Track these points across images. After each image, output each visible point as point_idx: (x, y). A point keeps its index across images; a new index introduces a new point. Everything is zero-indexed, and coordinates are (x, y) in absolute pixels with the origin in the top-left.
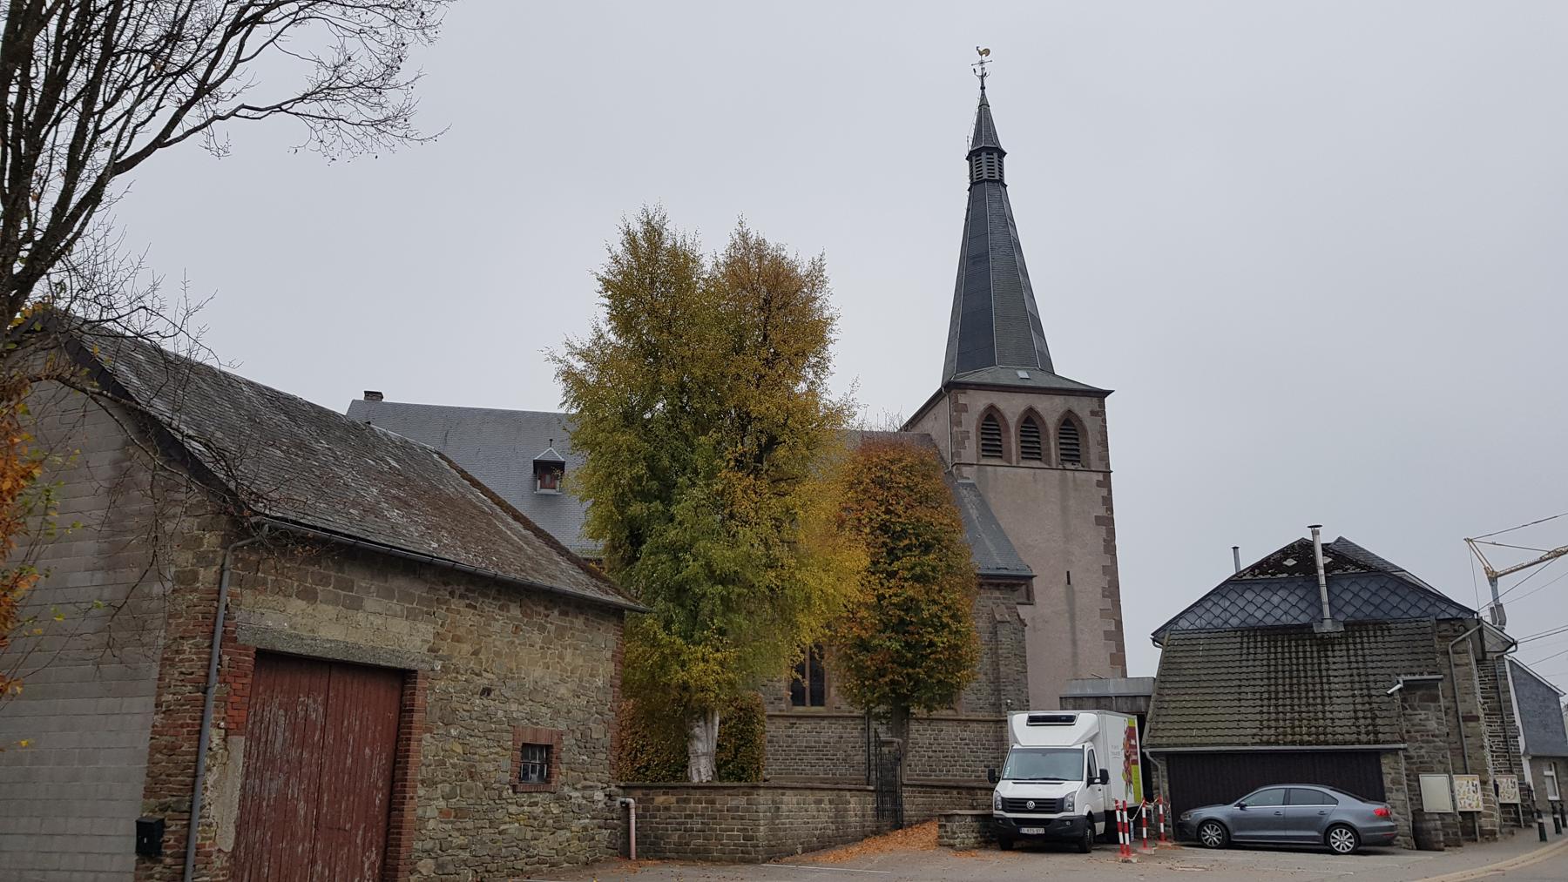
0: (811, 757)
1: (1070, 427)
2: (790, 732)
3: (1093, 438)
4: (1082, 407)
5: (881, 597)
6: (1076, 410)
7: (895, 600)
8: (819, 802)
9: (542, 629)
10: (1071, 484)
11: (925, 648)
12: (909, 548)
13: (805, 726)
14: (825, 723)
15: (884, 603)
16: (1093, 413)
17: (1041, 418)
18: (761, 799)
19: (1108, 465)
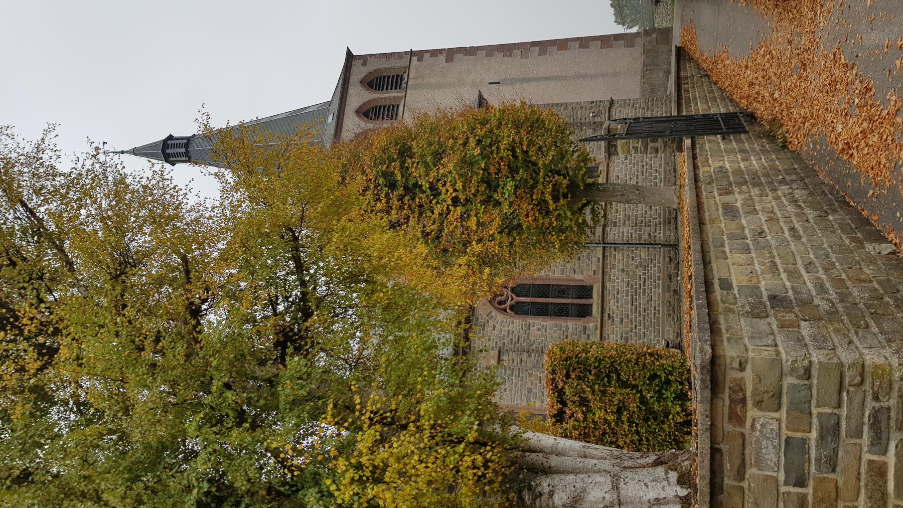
0: (642, 300)
1: (375, 82)
2: (617, 320)
3: (383, 64)
4: (359, 72)
5: (455, 201)
6: (361, 77)
7: (459, 185)
8: (730, 211)
9: (551, 494)
10: (419, 81)
11: (515, 156)
12: (404, 169)
13: (611, 305)
14: (609, 285)
15: (462, 197)
16: (364, 64)
17: (364, 104)
18: (759, 354)
19: (406, 53)
